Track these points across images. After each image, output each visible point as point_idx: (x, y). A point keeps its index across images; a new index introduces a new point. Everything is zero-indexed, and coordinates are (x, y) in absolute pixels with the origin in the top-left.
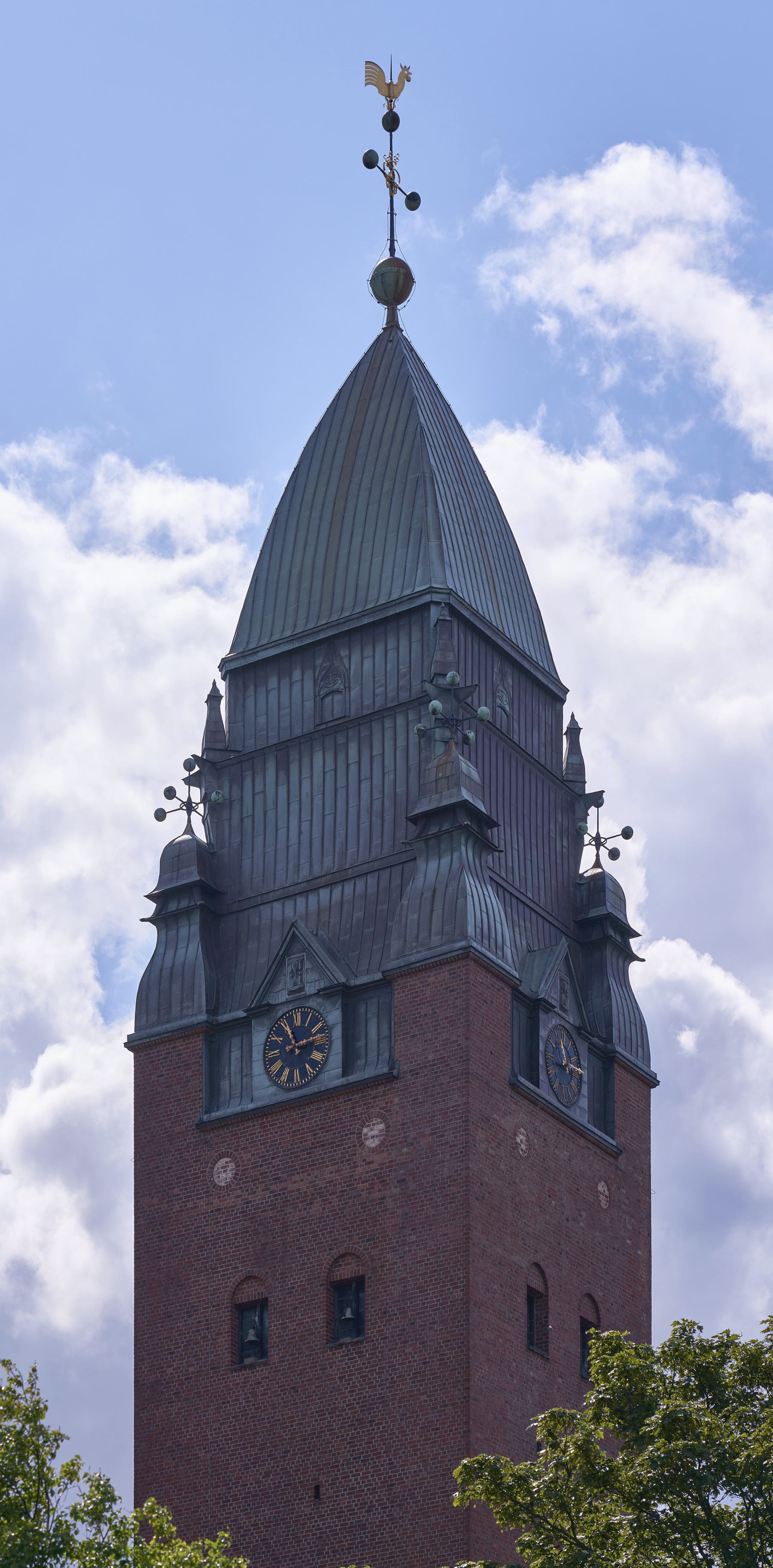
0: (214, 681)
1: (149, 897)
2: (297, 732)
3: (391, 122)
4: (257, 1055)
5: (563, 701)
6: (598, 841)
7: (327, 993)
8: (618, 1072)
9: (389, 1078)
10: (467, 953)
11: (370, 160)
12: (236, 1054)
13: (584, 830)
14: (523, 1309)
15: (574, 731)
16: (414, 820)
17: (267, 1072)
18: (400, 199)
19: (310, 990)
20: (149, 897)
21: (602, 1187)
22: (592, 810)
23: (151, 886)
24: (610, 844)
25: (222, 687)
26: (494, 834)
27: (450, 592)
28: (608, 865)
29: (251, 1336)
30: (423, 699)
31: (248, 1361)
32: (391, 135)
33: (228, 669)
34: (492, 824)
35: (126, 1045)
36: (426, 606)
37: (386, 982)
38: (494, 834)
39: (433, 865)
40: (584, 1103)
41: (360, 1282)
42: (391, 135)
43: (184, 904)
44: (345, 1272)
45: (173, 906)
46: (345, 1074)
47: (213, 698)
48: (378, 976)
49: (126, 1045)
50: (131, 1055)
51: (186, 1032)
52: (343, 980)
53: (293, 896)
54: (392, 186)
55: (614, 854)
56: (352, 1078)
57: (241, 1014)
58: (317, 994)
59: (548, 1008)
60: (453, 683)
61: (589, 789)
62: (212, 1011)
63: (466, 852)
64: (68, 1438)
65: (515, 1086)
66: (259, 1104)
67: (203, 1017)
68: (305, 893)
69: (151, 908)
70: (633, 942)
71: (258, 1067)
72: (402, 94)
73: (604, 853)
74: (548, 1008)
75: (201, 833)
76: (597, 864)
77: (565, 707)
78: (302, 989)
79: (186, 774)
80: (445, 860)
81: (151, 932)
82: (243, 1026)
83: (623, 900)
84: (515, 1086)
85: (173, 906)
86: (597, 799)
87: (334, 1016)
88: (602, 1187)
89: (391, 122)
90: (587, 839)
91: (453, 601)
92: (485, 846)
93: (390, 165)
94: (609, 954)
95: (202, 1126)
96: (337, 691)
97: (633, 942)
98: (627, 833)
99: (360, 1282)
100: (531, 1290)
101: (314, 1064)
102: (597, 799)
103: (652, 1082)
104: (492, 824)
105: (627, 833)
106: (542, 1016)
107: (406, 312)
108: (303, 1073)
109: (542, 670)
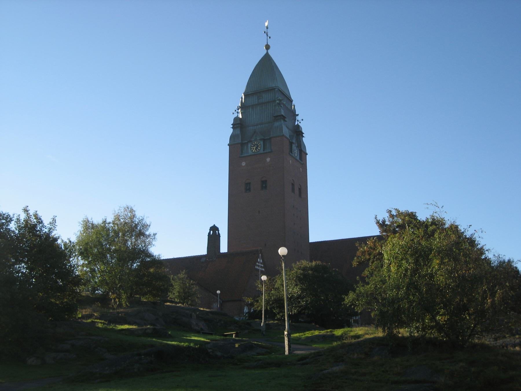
1: (232, 125)
2: (255, 104)
4: (249, 148)
5: (292, 102)
7: (261, 140)
8: (303, 153)
9: (271, 152)
10: (283, 135)
12: (245, 147)
13: (296, 119)
15: (294, 106)
16: (274, 117)
17: (251, 150)
18: (268, 38)
19: (258, 139)
20: (232, 125)
21: (301, 169)
22: (297, 117)
23: (232, 123)
26: (286, 119)
27: (278, 87)
28: (299, 124)
29: (248, 188)
30: (275, 101)
31: (247, 192)
32: (267, 43)
34: (286, 118)
35: (228, 145)
36: (275, 88)
37: (270, 139)
38: (286, 119)
39: (277, 123)
40: (298, 157)
41: (266, 181)
42: (267, 43)
43: (237, 126)
44: (264, 179)
45: (235, 126)
46: (263, 151)
47: (242, 98)
48: (269, 138)
49: (228, 145)
50: (229, 146)
51: (238, 144)
52: (263, 138)
53: (255, 126)
54: (267, 35)
55: (300, 122)
56: (265, 152)
57: (246, 142)
58: (259, 140)
59: (294, 143)
60: (280, 99)
61: (296, 114)
62: (242, 140)
63: (282, 121)
64: (36, 211)
65: (289, 154)
66: (250, 154)
67: (240, 142)
68: (256, 125)
69: (232, 126)
70: (303, 135)
71: (249, 149)
73: (299, 122)
74: (294, 143)
75: (240, 116)
76: (298, 124)
77: (293, 103)
78: (256, 139)
79: (237, 108)
80: (279, 123)
81: (232, 129)
82: (247, 143)
83: (302, 129)
84: (289, 154)
85: (235, 126)
86: (298, 115)
87: (262, 143)
88: (301, 169)
90: (296, 120)
91: (279, 88)
92: (285, 121)
93: (267, 33)
94: (300, 136)
95: (240, 157)
96: (261, 99)
97: (303, 135)
98: (302, 120)
99: (266, 181)
100: (292, 184)
101: (258, 149)
102: (298, 115)
103: (307, 154)
104: (286, 118)
106: (293, 145)
107: (269, 51)
108: (257, 150)
109: (289, 97)
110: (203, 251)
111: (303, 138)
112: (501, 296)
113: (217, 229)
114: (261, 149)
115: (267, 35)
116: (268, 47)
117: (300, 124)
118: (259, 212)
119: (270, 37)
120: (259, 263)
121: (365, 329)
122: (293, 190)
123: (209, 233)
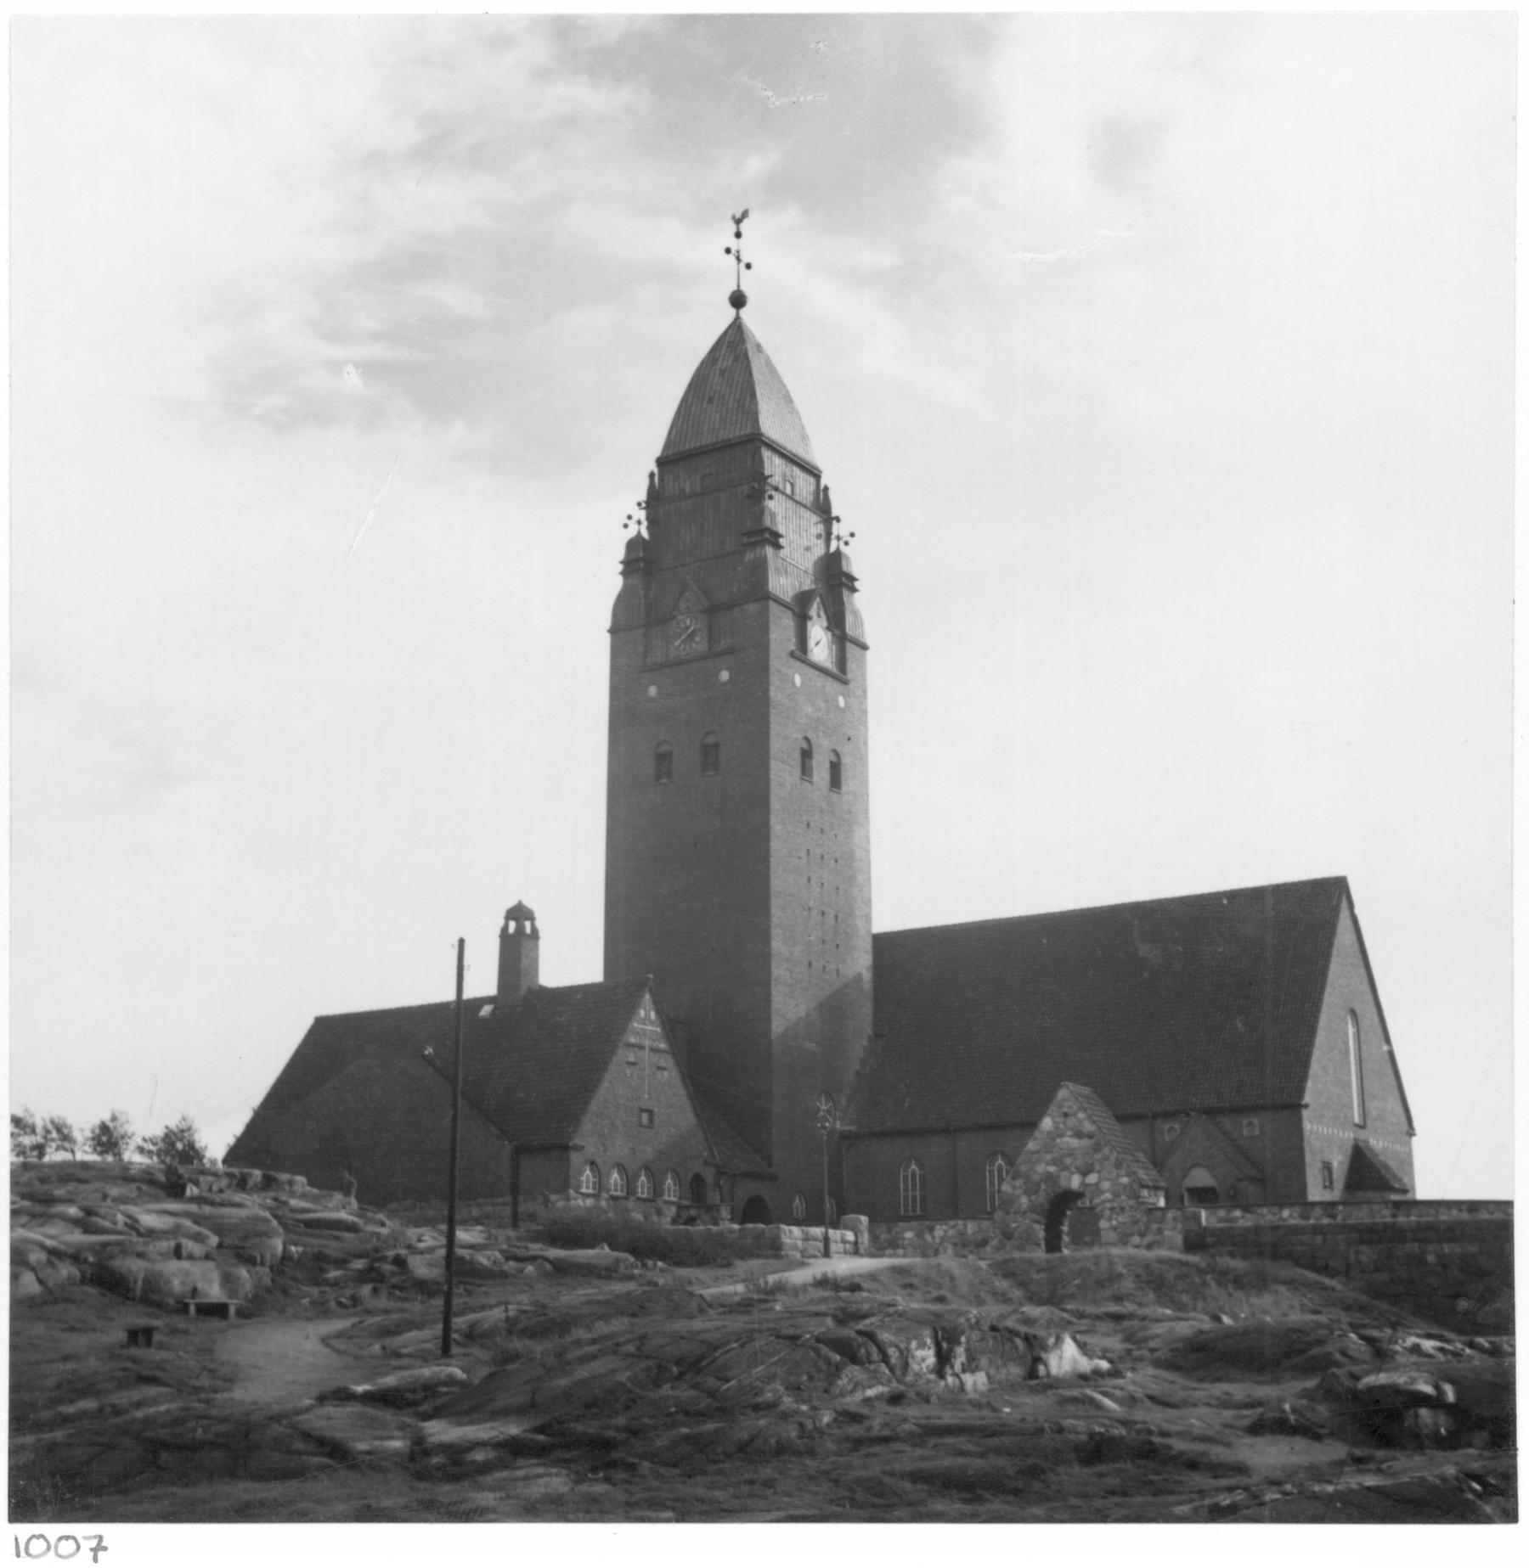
0: (518, 913)
3: (738, 235)
6: (838, 538)
11: (728, 251)
14: (799, 759)
18: (742, 265)
24: (844, 539)
25: (656, 470)
28: (843, 549)
32: (739, 286)
33: (660, 462)
42: (739, 286)
47: (652, 475)
54: (738, 259)
55: (846, 543)
72: (872, 871)
73: (842, 543)
75: (645, 534)
89: (738, 235)
94: (845, 592)
98: (852, 535)
99: (716, 746)
105: (852, 535)
107: (744, 313)
110: (449, 995)
111: (856, 595)
112: (962, 1320)
113: (530, 916)
114: (700, 645)
115: (738, 259)
116: (738, 300)
117: (847, 547)
118: (808, 825)
119: (748, 266)
120: (643, 1021)
121: (994, 1247)
122: (806, 771)
123: (505, 929)
